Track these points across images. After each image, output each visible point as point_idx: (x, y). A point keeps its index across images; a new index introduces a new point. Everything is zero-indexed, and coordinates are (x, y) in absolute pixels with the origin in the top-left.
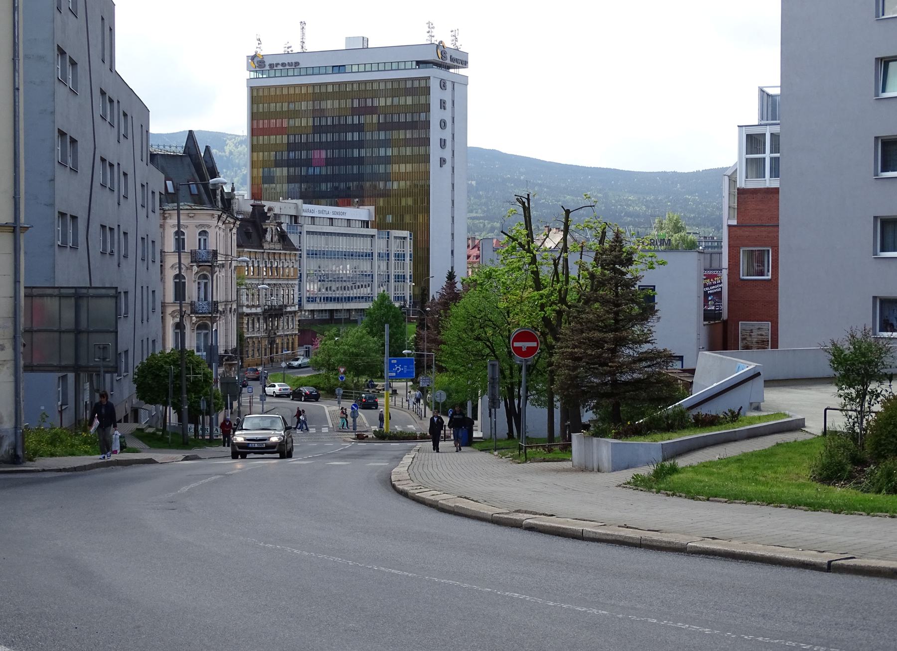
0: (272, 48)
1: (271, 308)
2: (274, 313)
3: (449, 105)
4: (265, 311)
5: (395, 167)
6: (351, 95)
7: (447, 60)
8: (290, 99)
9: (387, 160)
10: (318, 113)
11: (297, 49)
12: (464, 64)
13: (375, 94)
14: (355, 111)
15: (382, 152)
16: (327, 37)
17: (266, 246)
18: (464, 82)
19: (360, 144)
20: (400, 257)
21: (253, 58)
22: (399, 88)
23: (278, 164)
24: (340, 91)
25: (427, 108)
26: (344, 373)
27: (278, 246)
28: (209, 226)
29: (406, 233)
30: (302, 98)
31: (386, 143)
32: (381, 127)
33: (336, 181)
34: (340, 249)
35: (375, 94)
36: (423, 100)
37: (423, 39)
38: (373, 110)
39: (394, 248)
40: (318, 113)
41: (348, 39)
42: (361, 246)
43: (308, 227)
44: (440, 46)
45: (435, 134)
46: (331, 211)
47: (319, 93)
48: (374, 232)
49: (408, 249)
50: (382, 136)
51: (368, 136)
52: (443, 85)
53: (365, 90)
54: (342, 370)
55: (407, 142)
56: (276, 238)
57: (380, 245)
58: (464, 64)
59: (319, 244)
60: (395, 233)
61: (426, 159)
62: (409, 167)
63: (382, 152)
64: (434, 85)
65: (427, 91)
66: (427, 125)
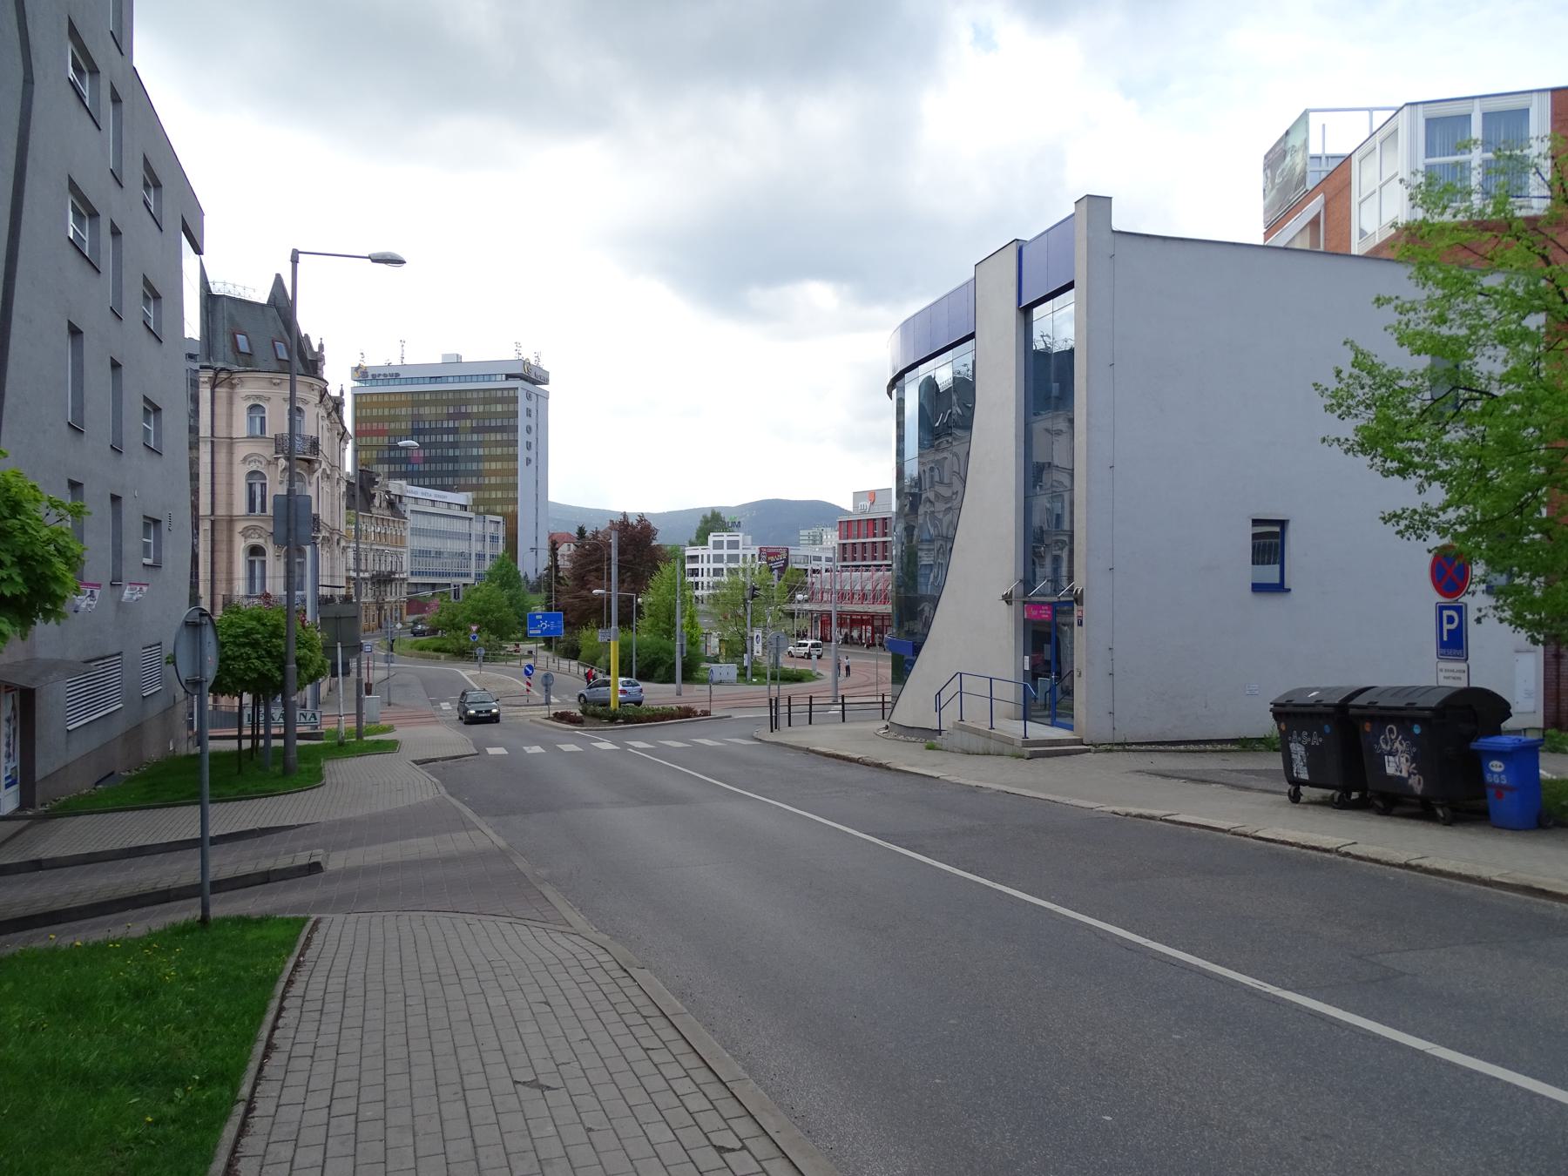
0: (374, 360)
1: (379, 574)
2: (383, 580)
3: (533, 414)
4: (373, 577)
5: (487, 465)
6: (447, 403)
7: (532, 377)
8: (391, 405)
9: (479, 459)
10: (416, 418)
11: (396, 362)
12: (546, 382)
13: (467, 402)
14: (450, 417)
15: (475, 451)
16: (424, 351)
17: (374, 510)
18: (546, 396)
19: (455, 445)
20: (494, 539)
21: (357, 369)
22: (489, 397)
23: (380, 461)
24: (437, 398)
25: (515, 414)
26: (478, 631)
27: (387, 512)
28: (306, 402)
29: (499, 519)
30: (402, 404)
31: (479, 444)
32: (474, 430)
33: (439, 468)
34: (438, 530)
35: (467, 402)
36: (511, 408)
37: (512, 356)
38: (467, 416)
39: (491, 529)
40: (416, 418)
41: (444, 356)
42: (459, 526)
43: (411, 506)
44: (525, 363)
45: (522, 437)
46: (433, 494)
47: (416, 400)
48: (472, 515)
49: (501, 533)
50: (475, 438)
51: (463, 438)
52: (529, 397)
53: (460, 398)
54: (474, 628)
55: (497, 444)
56: (384, 504)
57: (477, 527)
58: (546, 382)
59: (423, 522)
60: (489, 517)
61: (515, 458)
62: (499, 465)
63: (475, 451)
64: (521, 395)
65: (515, 400)
66: (515, 429)
